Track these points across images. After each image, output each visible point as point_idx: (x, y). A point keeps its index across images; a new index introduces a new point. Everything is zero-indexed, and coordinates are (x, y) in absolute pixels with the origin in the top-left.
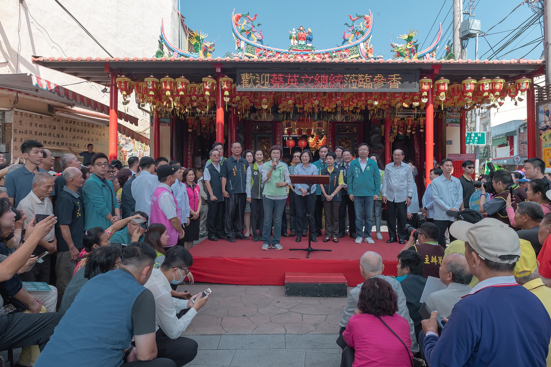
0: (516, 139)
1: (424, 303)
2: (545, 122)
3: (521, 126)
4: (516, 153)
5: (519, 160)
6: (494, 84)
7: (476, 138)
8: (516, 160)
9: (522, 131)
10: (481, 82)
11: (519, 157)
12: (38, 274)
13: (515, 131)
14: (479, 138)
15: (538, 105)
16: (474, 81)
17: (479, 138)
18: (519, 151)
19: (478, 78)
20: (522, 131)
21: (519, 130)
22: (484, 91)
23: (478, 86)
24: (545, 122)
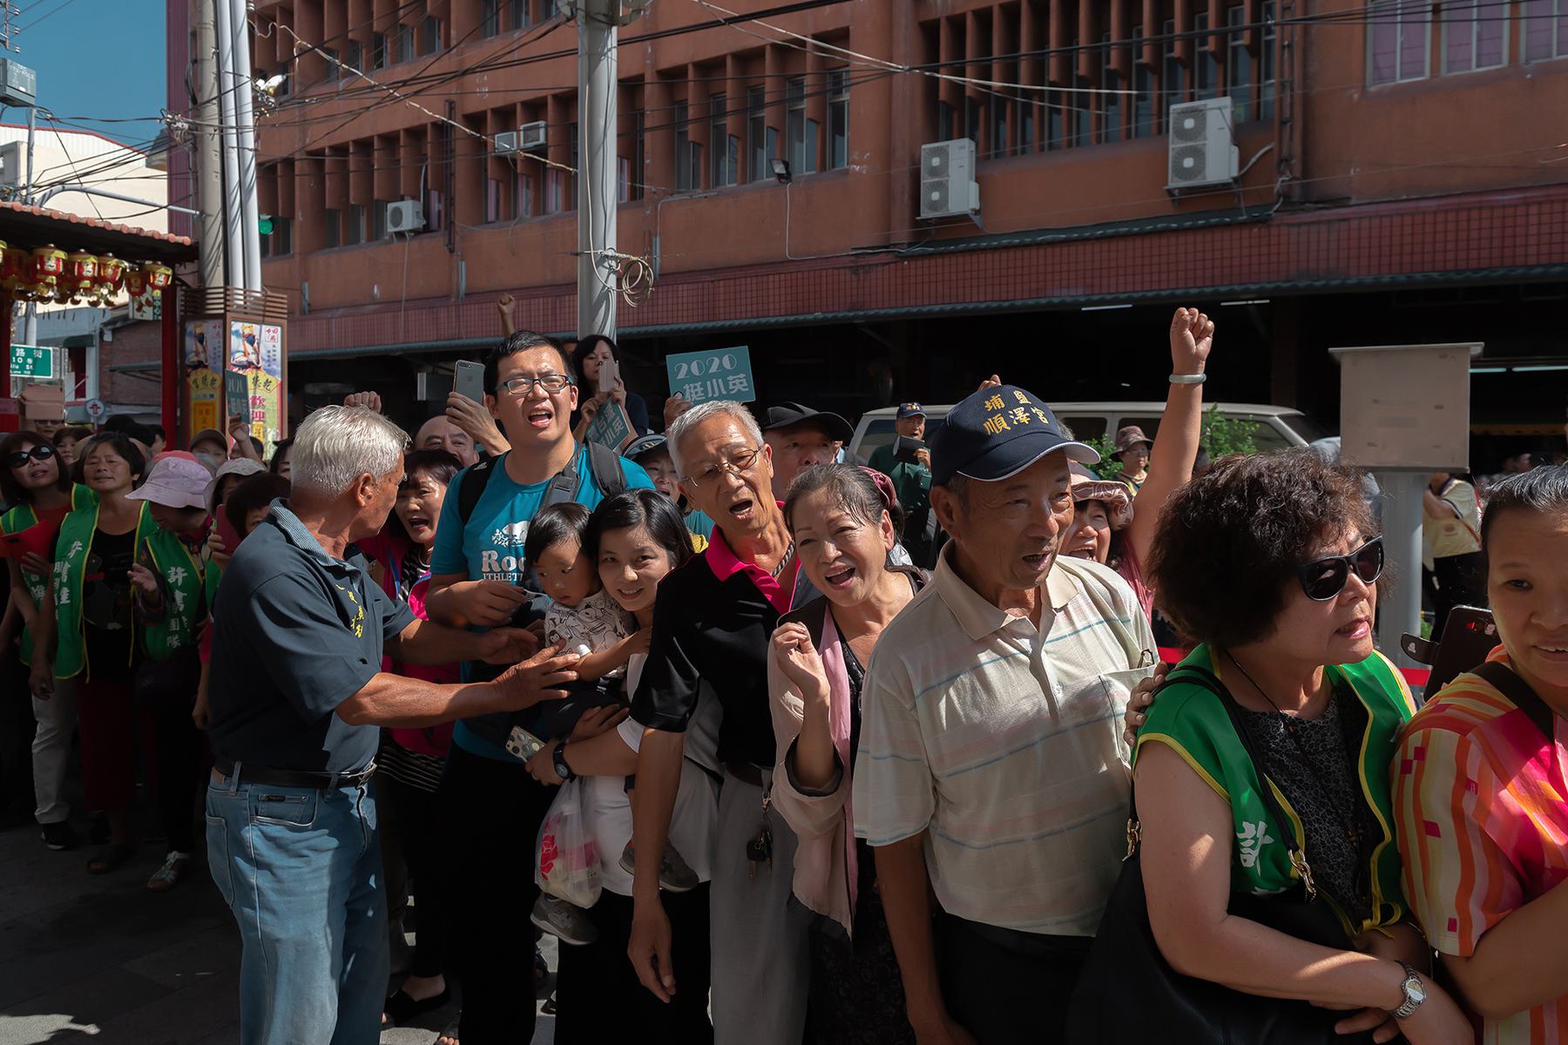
0: (92, 356)
1: (1436, 561)
2: (197, 354)
3: (106, 324)
4: (91, 392)
5: (100, 411)
6: (102, 266)
7: (30, 361)
8: (91, 412)
9: (108, 337)
10: (78, 259)
11: (100, 404)
12: (532, 718)
13: (90, 337)
14: (35, 360)
15: (184, 320)
16: (62, 255)
17: (35, 360)
18: (101, 387)
19: (71, 249)
20: (108, 337)
21: (102, 334)
22: (82, 278)
23: (68, 265)
24: (197, 354)
